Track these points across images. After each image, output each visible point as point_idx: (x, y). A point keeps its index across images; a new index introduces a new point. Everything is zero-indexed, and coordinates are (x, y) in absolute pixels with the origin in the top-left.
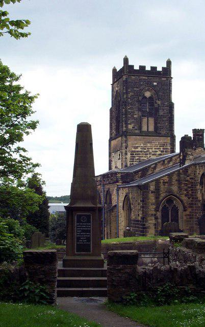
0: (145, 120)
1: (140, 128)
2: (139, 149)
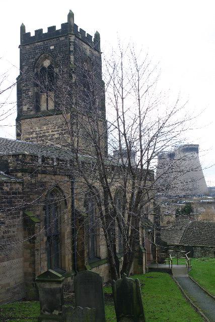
0: (44, 97)
1: (37, 108)
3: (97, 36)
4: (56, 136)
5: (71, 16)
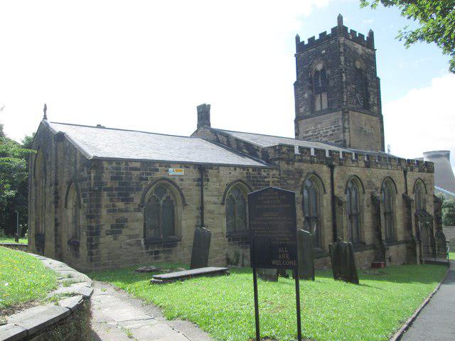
0: (318, 98)
2: (310, 133)
3: (371, 34)
5: (340, 19)
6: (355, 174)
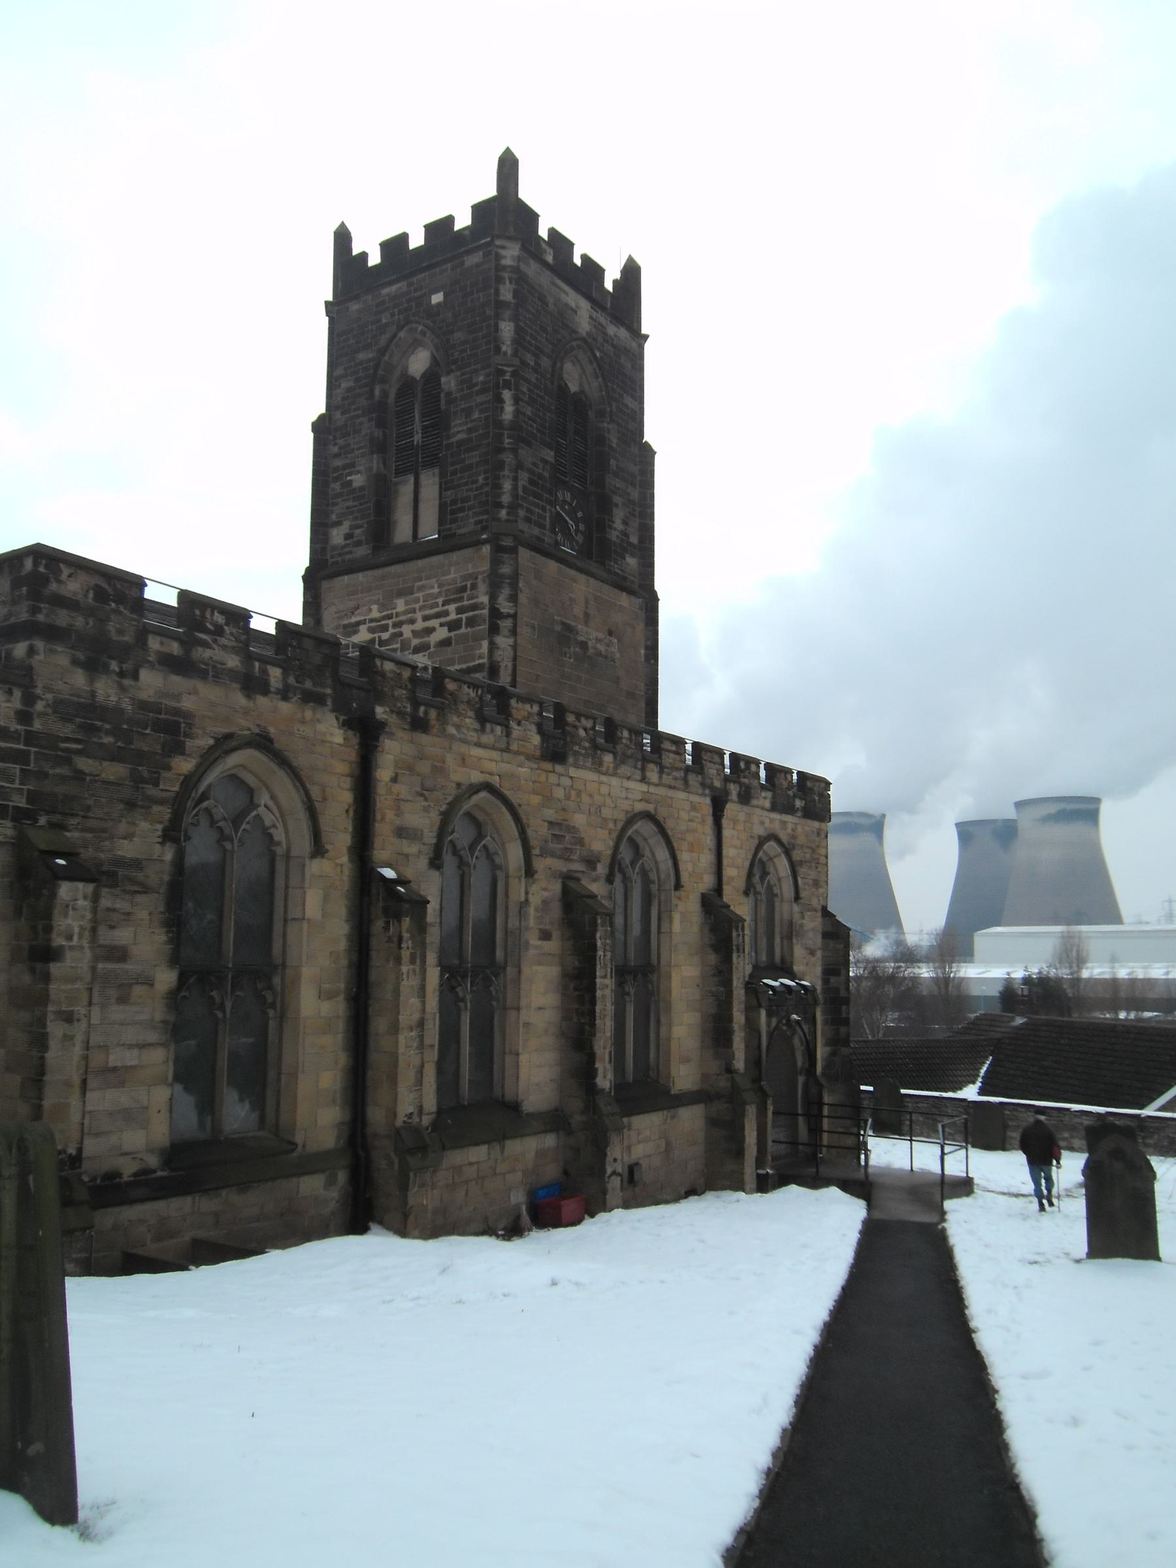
3: (631, 272)
4: (442, 633)
5: (508, 167)
6: (488, 778)
